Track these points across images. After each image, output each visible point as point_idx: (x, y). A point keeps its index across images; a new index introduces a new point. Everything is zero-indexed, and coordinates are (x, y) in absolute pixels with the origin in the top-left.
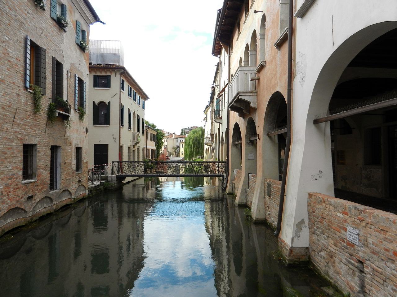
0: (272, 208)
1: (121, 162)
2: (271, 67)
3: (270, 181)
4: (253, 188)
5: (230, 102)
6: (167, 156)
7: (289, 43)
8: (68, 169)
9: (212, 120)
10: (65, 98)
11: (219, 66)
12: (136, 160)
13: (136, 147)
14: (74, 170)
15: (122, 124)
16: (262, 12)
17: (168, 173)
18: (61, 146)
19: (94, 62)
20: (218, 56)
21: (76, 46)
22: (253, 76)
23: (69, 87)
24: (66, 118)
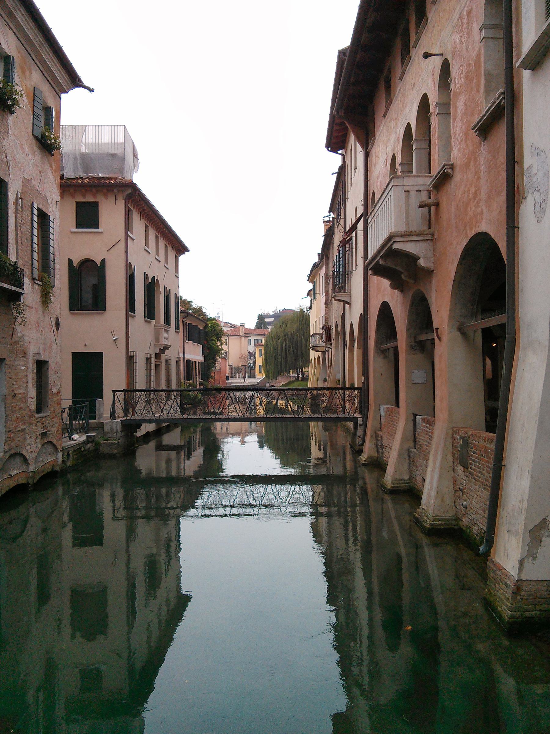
0: (472, 494)
1: (129, 392)
2: (465, 177)
3: (466, 433)
4: (425, 447)
5: (370, 256)
6: (227, 375)
7: (507, 128)
8: (21, 409)
9: (327, 295)
10: (12, 257)
11: (342, 173)
12: (163, 386)
13: (163, 357)
14: (32, 411)
15: (131, 307)
16: (441, 55)
17: (234, 414)
18: (5, 359)
19: (69, 173)
20: (340, 152)
21: (34, 141)
22: (424, 197)
23: (19, 232)
24: (17, 297)
